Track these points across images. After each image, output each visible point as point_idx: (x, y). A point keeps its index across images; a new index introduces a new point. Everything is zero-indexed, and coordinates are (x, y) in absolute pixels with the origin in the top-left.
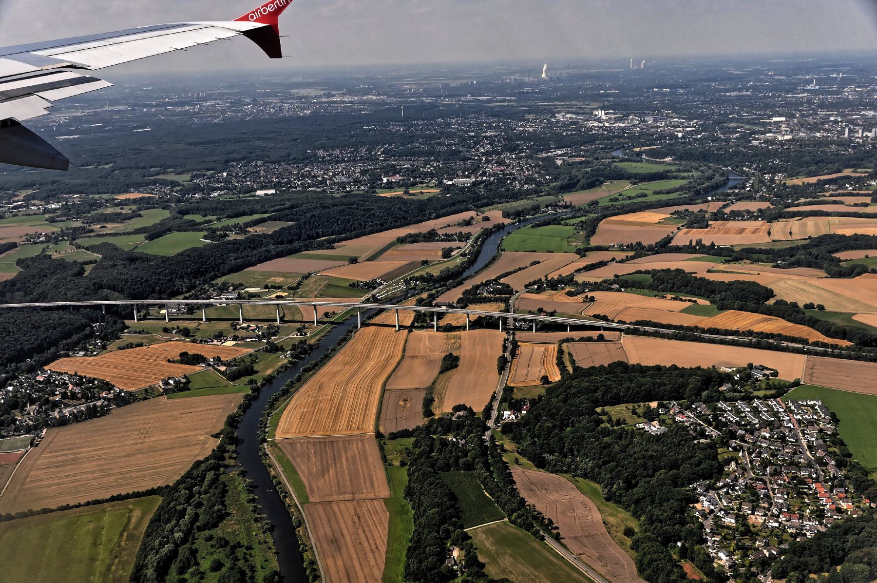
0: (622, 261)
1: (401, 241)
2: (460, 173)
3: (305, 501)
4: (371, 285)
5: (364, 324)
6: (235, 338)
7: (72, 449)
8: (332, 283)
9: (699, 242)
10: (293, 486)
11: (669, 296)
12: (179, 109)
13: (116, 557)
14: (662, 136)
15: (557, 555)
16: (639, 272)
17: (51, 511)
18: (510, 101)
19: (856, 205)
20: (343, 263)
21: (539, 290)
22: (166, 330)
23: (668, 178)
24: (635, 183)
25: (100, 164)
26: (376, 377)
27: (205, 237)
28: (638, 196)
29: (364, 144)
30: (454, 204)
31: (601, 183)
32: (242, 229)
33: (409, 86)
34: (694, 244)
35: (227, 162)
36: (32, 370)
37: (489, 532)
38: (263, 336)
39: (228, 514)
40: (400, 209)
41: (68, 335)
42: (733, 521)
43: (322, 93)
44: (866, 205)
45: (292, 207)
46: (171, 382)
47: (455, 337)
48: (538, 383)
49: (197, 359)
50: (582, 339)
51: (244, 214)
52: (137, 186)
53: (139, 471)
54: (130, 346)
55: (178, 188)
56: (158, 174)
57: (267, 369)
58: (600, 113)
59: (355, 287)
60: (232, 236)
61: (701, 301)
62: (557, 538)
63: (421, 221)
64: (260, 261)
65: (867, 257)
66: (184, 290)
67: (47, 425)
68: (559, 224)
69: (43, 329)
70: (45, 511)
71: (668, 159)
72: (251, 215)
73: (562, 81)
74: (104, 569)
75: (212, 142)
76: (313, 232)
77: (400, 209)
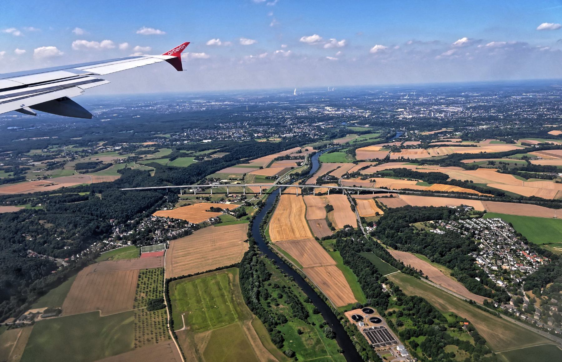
0: (375, 166)
1: (277, 159)
2: (285, 132)
3: (302, 267)
4: (275, 178)
5: (282, 194)
6: (230, 201)
7: (185, 249)
8: (257, 177)
9: (402, 158)
10: (293, 261)
11: (406, 179)
12: (147, 108)
13: (233, 294)
14: (359, 117)
15: (431, 285)
16: (387, 170)
17: (192, 275)
18: (286, 104)
19: (457, 142)
20: (257, 169)
21: (348, 178)
22: (197, 198)
23: (371, 133)
24: (359, 135)
25: (127, 131)
26: (300, 215)
27: (195, 159)
28: (363, 140)
29: (238, 121)
30: (291, 145)
31: (346, 135)
32: (209, 155)
33: (242, 99)
34: (400, 158)
35: (183, 129)
36: (148, 216)
37: (394, 276)
38: (242, 199)
39: (271, 274)
40: (271, 146)
41: (157, 201)
42: (497, 268)
43: (205, 101)
44: (461, 142)
45: (225, 146)
46: (213, 219)
47: (324, 198)
48: (374, 215)
49: (219, 210)
50: (383, 197)
51: (205, 150)
52: (150, 139)
53: (220, 257)
54: (185, 205)
55: (168, 140)
56: (155, 134)
57: (253, 211)
58: (328, 108)
59: (268, 179)
60: (206, 159)
61: (420, 181)
62: (427, 278)
63: (280, 152)
64: (221, 169)
65: (474, 162)
66: (196, 181)
67: (168, 239)
68: (338, 152)
69: (147, 199)
70: (189, 276)
71: (367, 126)
72: (208, 150)
73: (304, 96)
74: (230, 299)
75: (172, 121)
76: (237, 157)
77: (271, 146)
